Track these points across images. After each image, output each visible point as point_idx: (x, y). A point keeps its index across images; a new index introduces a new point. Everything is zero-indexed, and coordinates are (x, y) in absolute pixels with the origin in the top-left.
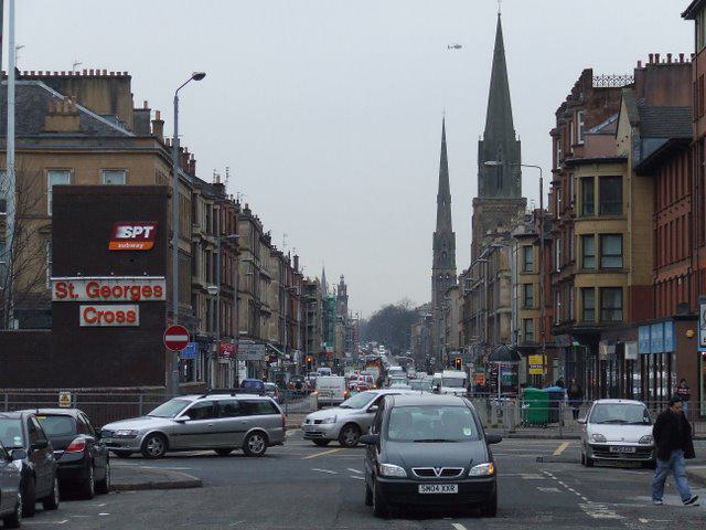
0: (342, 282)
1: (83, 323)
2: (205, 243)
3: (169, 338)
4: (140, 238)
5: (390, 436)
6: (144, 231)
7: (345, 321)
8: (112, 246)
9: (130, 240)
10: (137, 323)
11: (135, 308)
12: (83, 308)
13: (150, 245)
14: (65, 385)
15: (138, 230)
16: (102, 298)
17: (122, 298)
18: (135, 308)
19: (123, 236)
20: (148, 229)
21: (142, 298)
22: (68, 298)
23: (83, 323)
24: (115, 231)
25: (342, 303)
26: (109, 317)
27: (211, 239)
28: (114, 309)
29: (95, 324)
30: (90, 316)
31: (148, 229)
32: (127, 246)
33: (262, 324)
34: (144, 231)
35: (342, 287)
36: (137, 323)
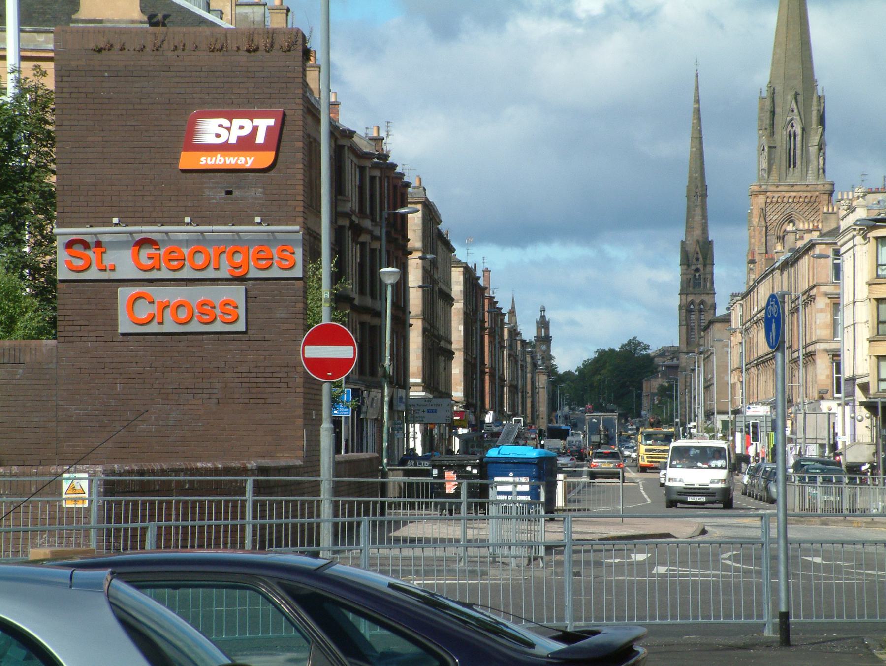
0: (543, 317)
1: (125, 325)
2: (357, 230)
3: (346, 352)
4: (246, 144)
5: (453, 491)
6: (255, 129)
7: (551, 370)
8: (188, 160)
9: (225, 147)
10: (240, 326)
11: (237, 294)
12: (124, 294)
13: (266, 158)
14: (75, 461)
15: (240, 127)
16: (165, 274)
17: (210, 273)
18: (237, 294)
19: (208, 138)
20: (264, 124)
21: (253, 273)
22: (93, 274)
23: (125, 325)
24: (191, 130)
25: (544, 347)
26: (183, 315)
27: (367, 223)
28: (196, 295)
29: (153, 328)
30: (143, 311)
31: (264, 124)
32: (219, 160)
33: (441, 369)
34: (255, 129)
35: (543, 324)
36: (240, 326)
